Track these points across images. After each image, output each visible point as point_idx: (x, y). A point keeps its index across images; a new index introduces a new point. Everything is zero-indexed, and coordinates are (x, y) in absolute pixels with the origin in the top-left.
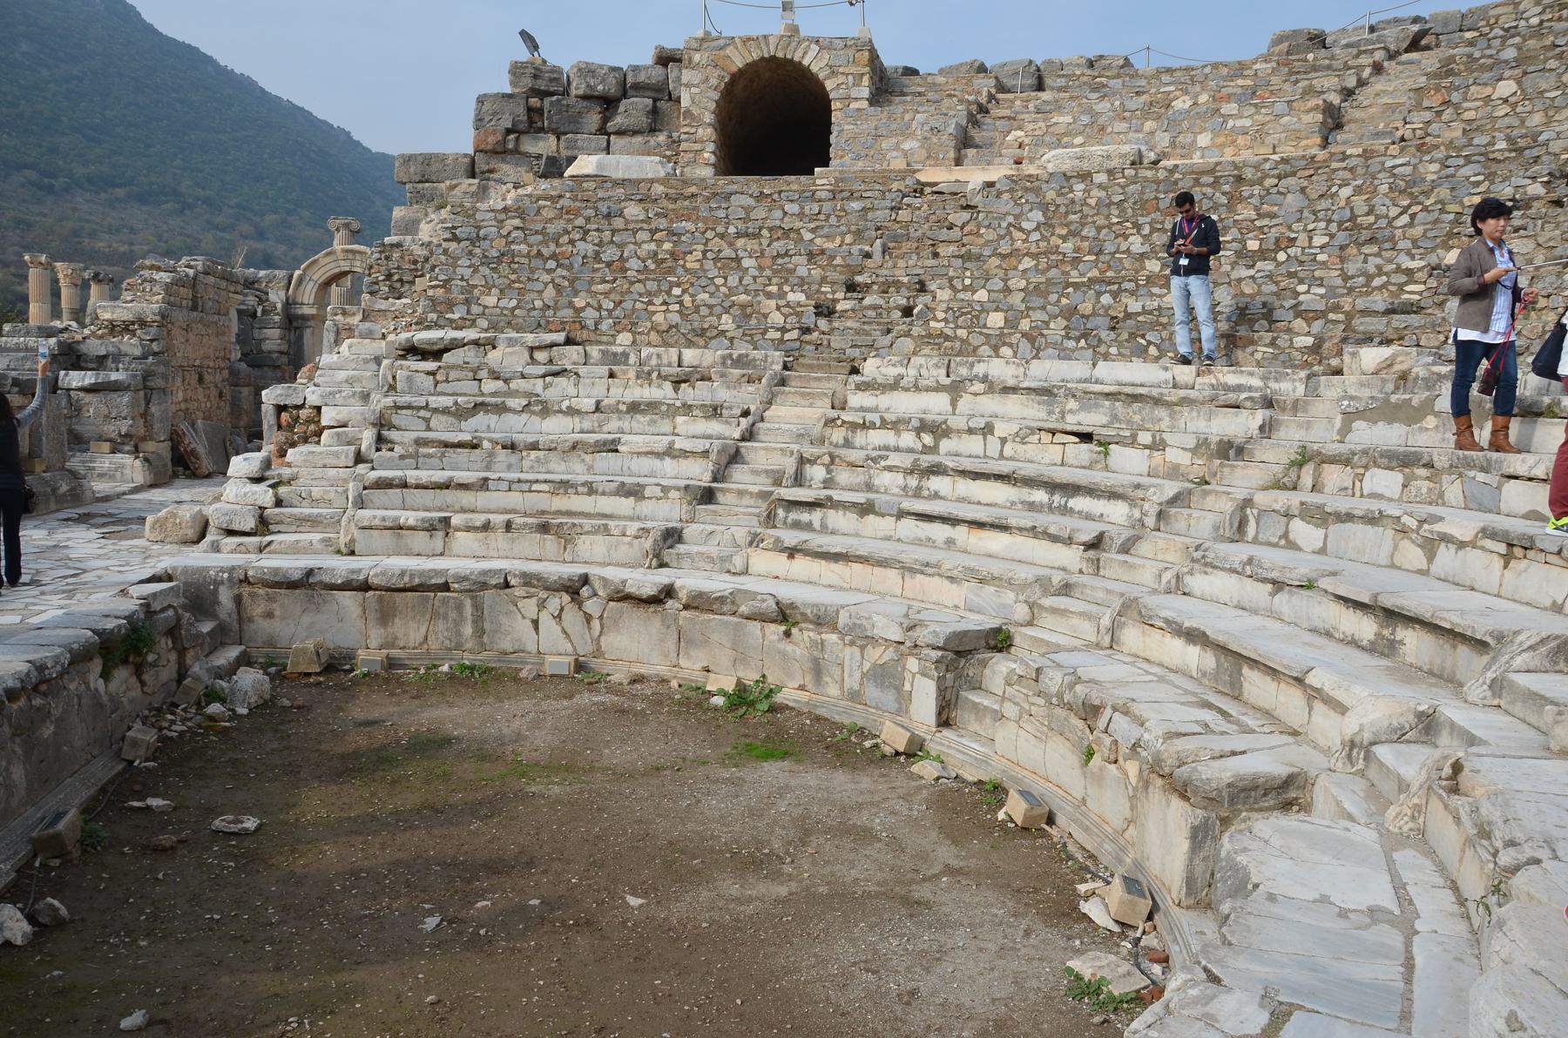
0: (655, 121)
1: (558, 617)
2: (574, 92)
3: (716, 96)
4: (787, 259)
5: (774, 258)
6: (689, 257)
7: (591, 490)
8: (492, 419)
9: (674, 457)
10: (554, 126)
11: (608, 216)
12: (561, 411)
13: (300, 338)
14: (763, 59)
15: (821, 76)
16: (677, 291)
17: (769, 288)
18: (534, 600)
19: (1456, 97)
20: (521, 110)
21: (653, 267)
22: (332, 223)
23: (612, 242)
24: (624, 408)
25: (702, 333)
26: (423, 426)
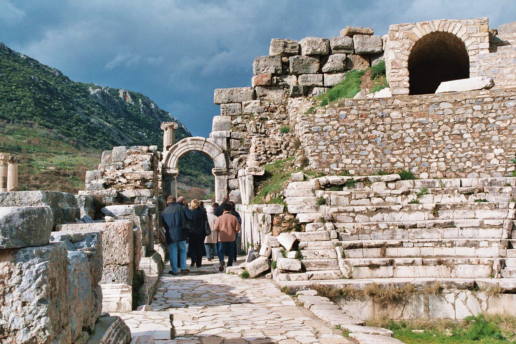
0: (347, 65)
1: (465, 302)
2: (304, 52)
3: (409, 53)
4: (487, 133)
5: (480, 133)
6: (436, 135)
7: (453, 244)
8: (386, 215)
9: (484, 228)
10: (295, 71)
11: (382, 117)
12: (418, 210)
13: (169, 185)
14: (432, 33)
15: (463, 40)
16: (436, 152)
17: (484, 148)
18: (453, 295)
20: (279, 64)
21: (418, 140)
22: (163, 126)
23: (391, 130)
24: (449, 207)
25: (463, 170)
26: (351, 220)
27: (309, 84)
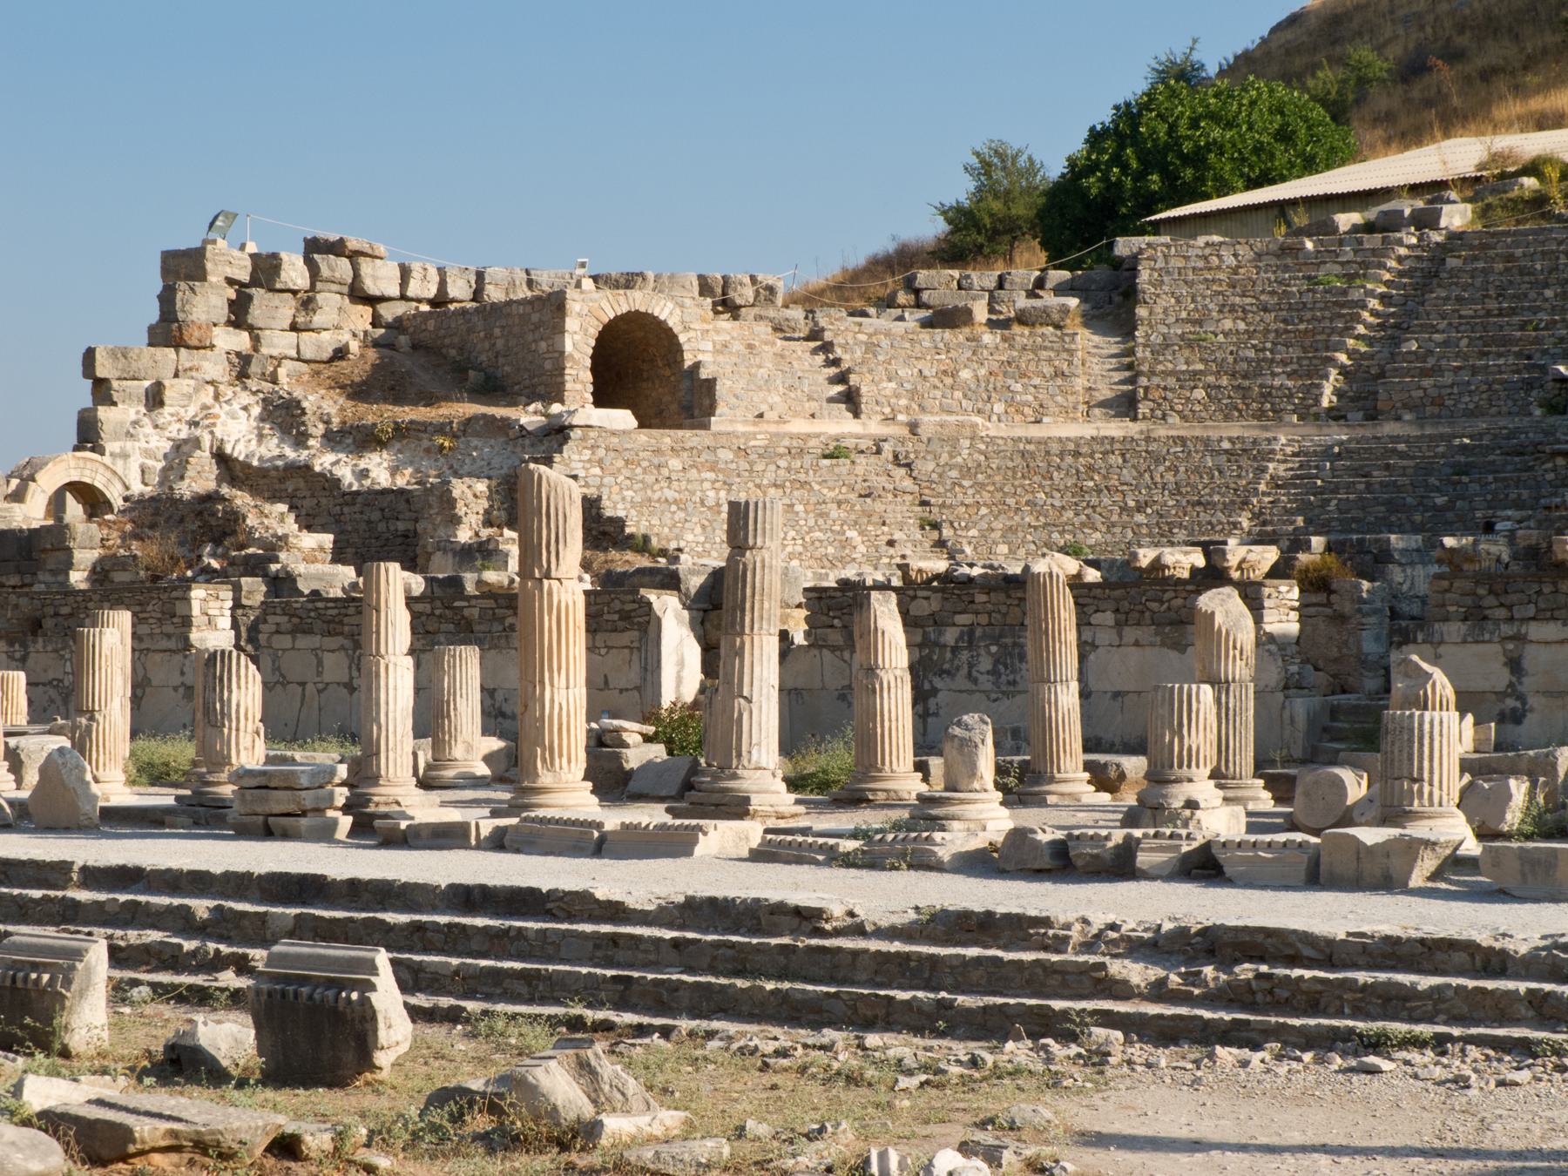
3: (593, 343)
19: (1170, 395)
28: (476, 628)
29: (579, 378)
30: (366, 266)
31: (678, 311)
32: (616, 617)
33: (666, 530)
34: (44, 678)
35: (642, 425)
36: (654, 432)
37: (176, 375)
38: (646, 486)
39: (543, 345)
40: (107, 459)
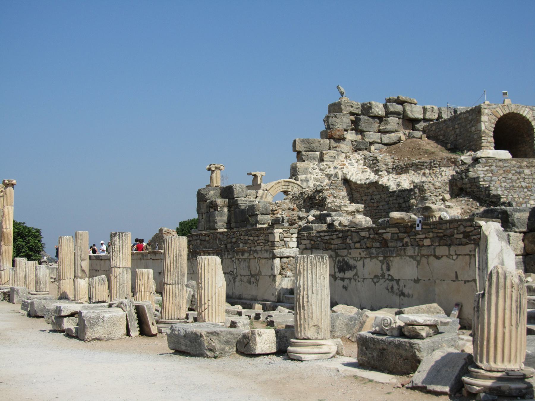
3: (494, 126)
27: (371, 141)
28: (390, 244)
29: (488, 139)
30: (408, 107)
31: (531, 112)
32: (461, 236)
33: (521, 200)
34: (228, 272)
35: (513, 157)
36: (519, 160)
37: (330, 149)
38: (513, 181)
39: (473, 128)
40: (299, 182)
